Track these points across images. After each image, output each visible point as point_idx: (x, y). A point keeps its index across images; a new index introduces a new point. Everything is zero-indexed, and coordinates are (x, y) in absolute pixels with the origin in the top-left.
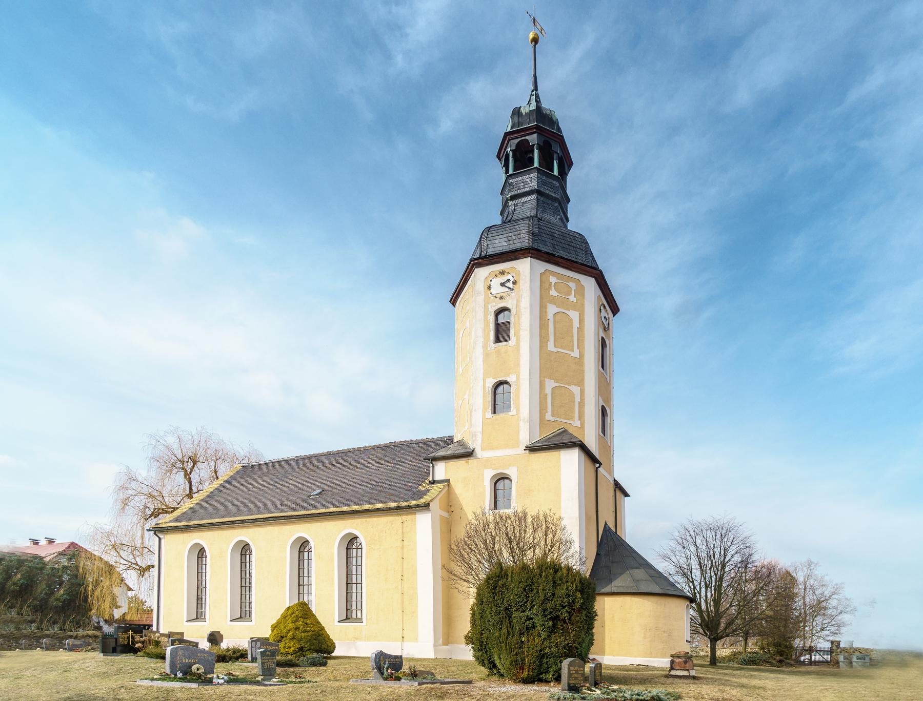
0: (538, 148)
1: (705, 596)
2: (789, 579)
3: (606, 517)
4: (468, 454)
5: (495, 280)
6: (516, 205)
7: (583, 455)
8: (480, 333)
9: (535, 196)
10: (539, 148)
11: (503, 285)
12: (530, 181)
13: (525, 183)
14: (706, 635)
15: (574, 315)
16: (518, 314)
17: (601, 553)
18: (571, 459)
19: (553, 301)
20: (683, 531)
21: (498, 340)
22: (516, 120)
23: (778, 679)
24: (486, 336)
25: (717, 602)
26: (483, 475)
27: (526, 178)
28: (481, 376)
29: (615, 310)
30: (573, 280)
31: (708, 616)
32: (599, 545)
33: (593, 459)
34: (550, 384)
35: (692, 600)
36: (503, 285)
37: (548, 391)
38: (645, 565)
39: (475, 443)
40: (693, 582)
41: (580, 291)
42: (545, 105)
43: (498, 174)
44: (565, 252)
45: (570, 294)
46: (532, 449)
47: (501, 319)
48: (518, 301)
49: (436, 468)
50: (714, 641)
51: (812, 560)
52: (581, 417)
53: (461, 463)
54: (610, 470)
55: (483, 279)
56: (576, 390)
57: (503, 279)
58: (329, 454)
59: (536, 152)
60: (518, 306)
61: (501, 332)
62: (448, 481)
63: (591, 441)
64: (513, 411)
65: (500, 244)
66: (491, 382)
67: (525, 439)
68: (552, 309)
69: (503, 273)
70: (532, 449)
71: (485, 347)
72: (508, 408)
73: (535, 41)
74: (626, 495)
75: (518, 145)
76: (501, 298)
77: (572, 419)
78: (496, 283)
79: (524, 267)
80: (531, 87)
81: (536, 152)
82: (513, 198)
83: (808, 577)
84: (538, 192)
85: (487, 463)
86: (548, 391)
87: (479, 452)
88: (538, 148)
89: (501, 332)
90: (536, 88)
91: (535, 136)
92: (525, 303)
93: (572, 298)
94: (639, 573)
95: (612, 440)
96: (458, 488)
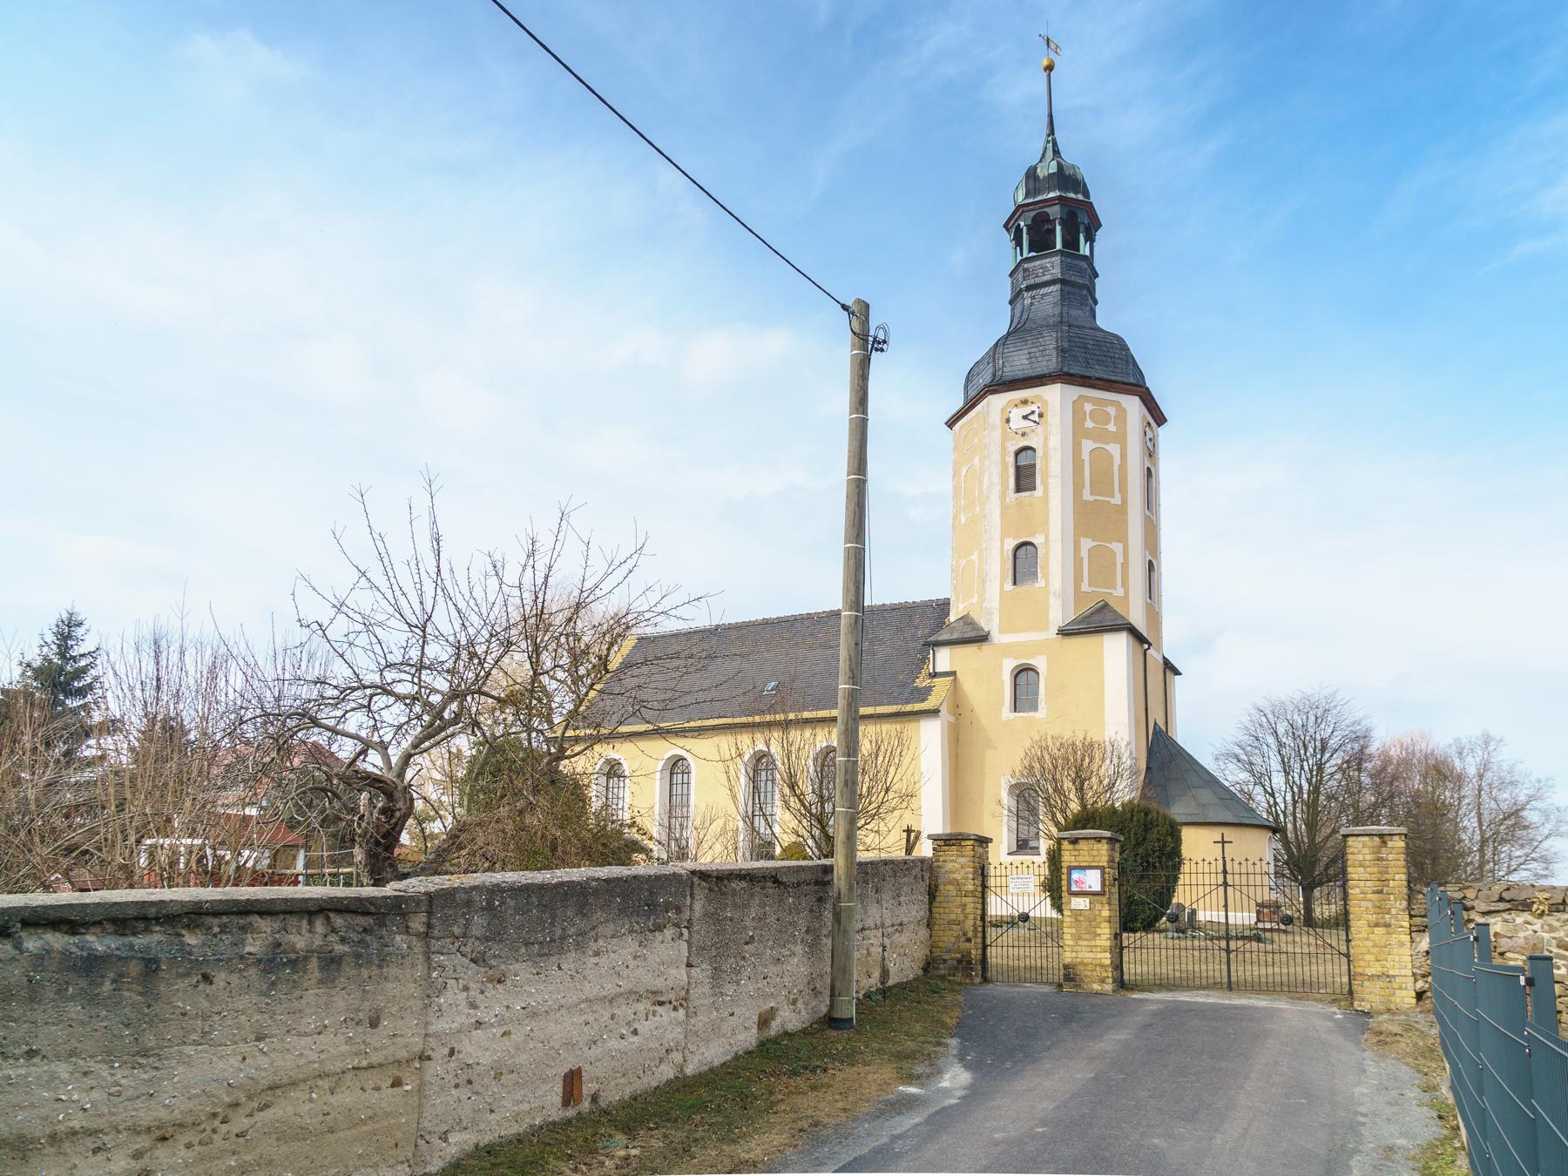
0: (1056, 220)
1: (1296, 826)
2: (1440, 771)
3: (1156, 715)
4: (983, 638)
5: (1015, 411)
6: (1033, 298)
7: (1131, 639)
8: (996, 479)
9: (1058, 287)
10: (1063, 223)
11: (1025, 417)
12: (1052, 266)
13: (1045, 269)
14: (1296, 880)
15: (1114, 449)
16: (1046, 456)
17: (1154, 766)
18: (1117, 646)
19: (1088, 434)
20: (1254, 712)
21: (1018, 489)
22: (1031, 185)
23: (1134, 772)
24: (1004, 483)
25: (1312, 825)
26: (1001, 666)
27: (1046, 262)
28: (998, 535)
29: (1160, 419)
30: (1112, 403)
31: (1299, 848)
32: (1150, 752)
33: (1139, 638)
34: (1087, 544)
35: (1275, 831)
36: (1025, 417)
37: (1084, 553)
38: (1211, 781)
39: (990, 623)
40: (1272, 795)
41: (1122, 418)
42: (1068, 157)
43: (1006, 254)
44: (1102, 366)
45: (1108, 422)
46: (1065, 633)
47: (1023, 461)
48: (1046, 439)
49: (938, 655)
50: (1308, 890)
51: (1492, 734)
52: (1125, 583)
53: (970, 650)
54: (1159, 649)
55: (999, 409)
56: (1117, 547)
57: (1026, 410)
58: (766, 623)
59: (1058, 228)
60: (1045, 445)
61: (1024, 478)
62: (953, 673)
63: (1138, 619)
64: (1041, 583)
65: (1019, 363)
66: (1011, 544)
67: (1058, 616)
68: (1088, 445)
69: (1025, 402)
70: (1065, 633)
71: (1003, 497)
72: (1033, 575)
73: (1049, 68)
74: (1177, 673)
75: (1034, 219)
76: (1023, 435)
77: (1114, 587)
78: (1016, 414)
79: (1053, 395)
80: (1045, 131)
81: (1058, 228)
82: (1029, 288)
83: (1484, 767)
84: (1063, 282)
85: (1008, 650)
86: (1084, 553)
87: (996, 637)
88: (1056, 220)
89: (1024, 478)
90: (1052, 132)
91: (1057, 208)
92: (1055, 442)
93: (1112, 427)
94: (1205, 795)
95: (1159, 603)
96: (967, 683)
